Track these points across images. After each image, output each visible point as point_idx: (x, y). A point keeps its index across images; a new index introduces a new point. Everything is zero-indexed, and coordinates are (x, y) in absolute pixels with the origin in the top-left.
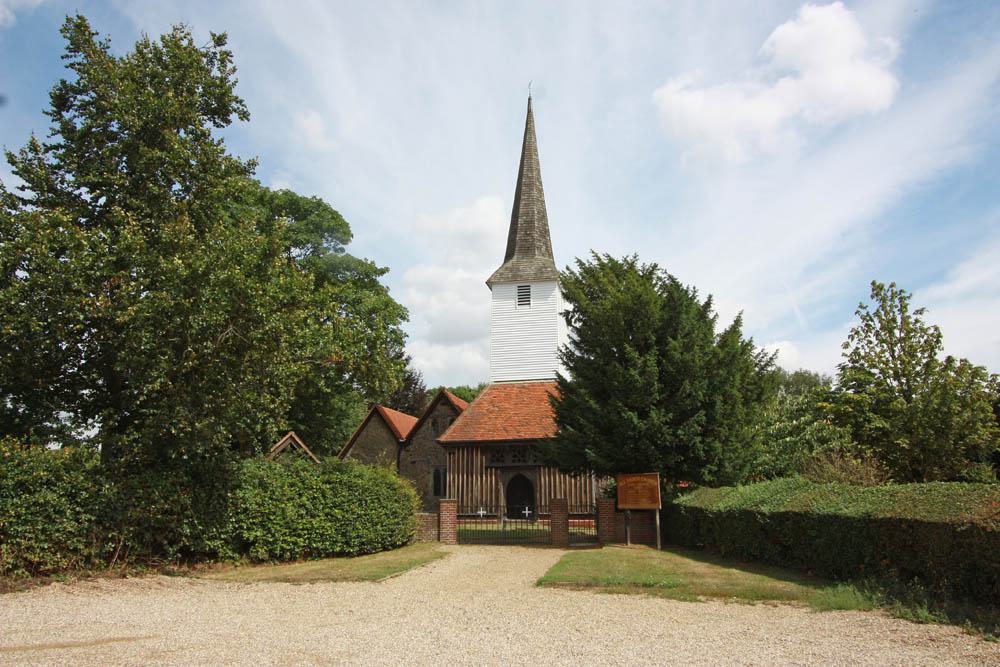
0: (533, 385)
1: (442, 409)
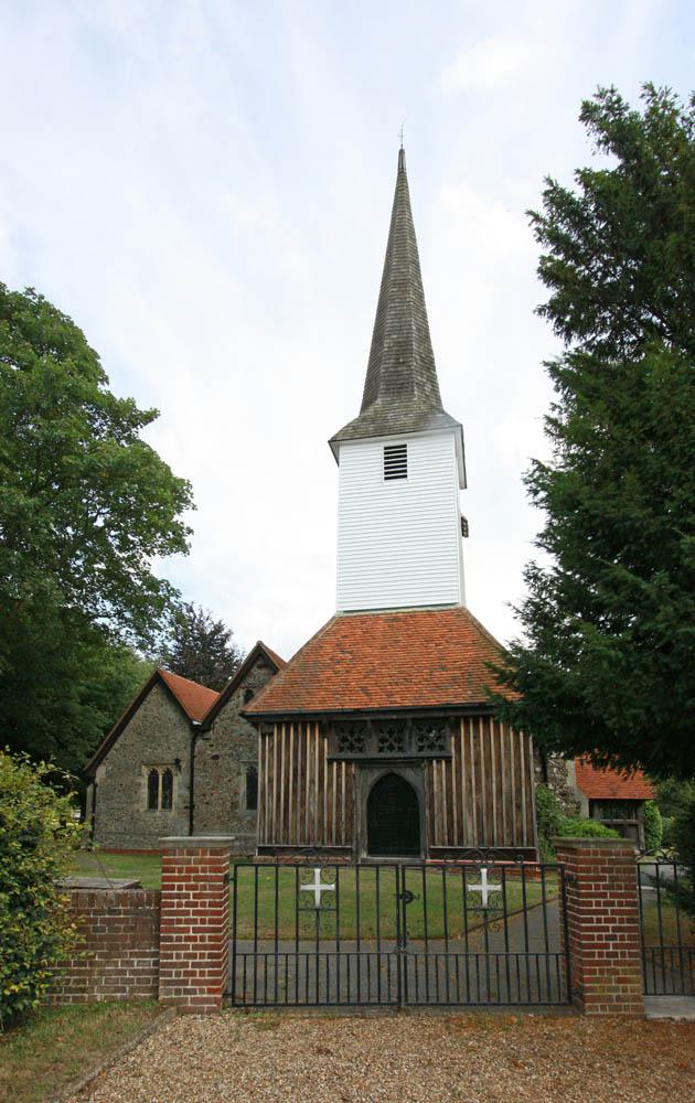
0: (413, 615)
1: (258, 673)
